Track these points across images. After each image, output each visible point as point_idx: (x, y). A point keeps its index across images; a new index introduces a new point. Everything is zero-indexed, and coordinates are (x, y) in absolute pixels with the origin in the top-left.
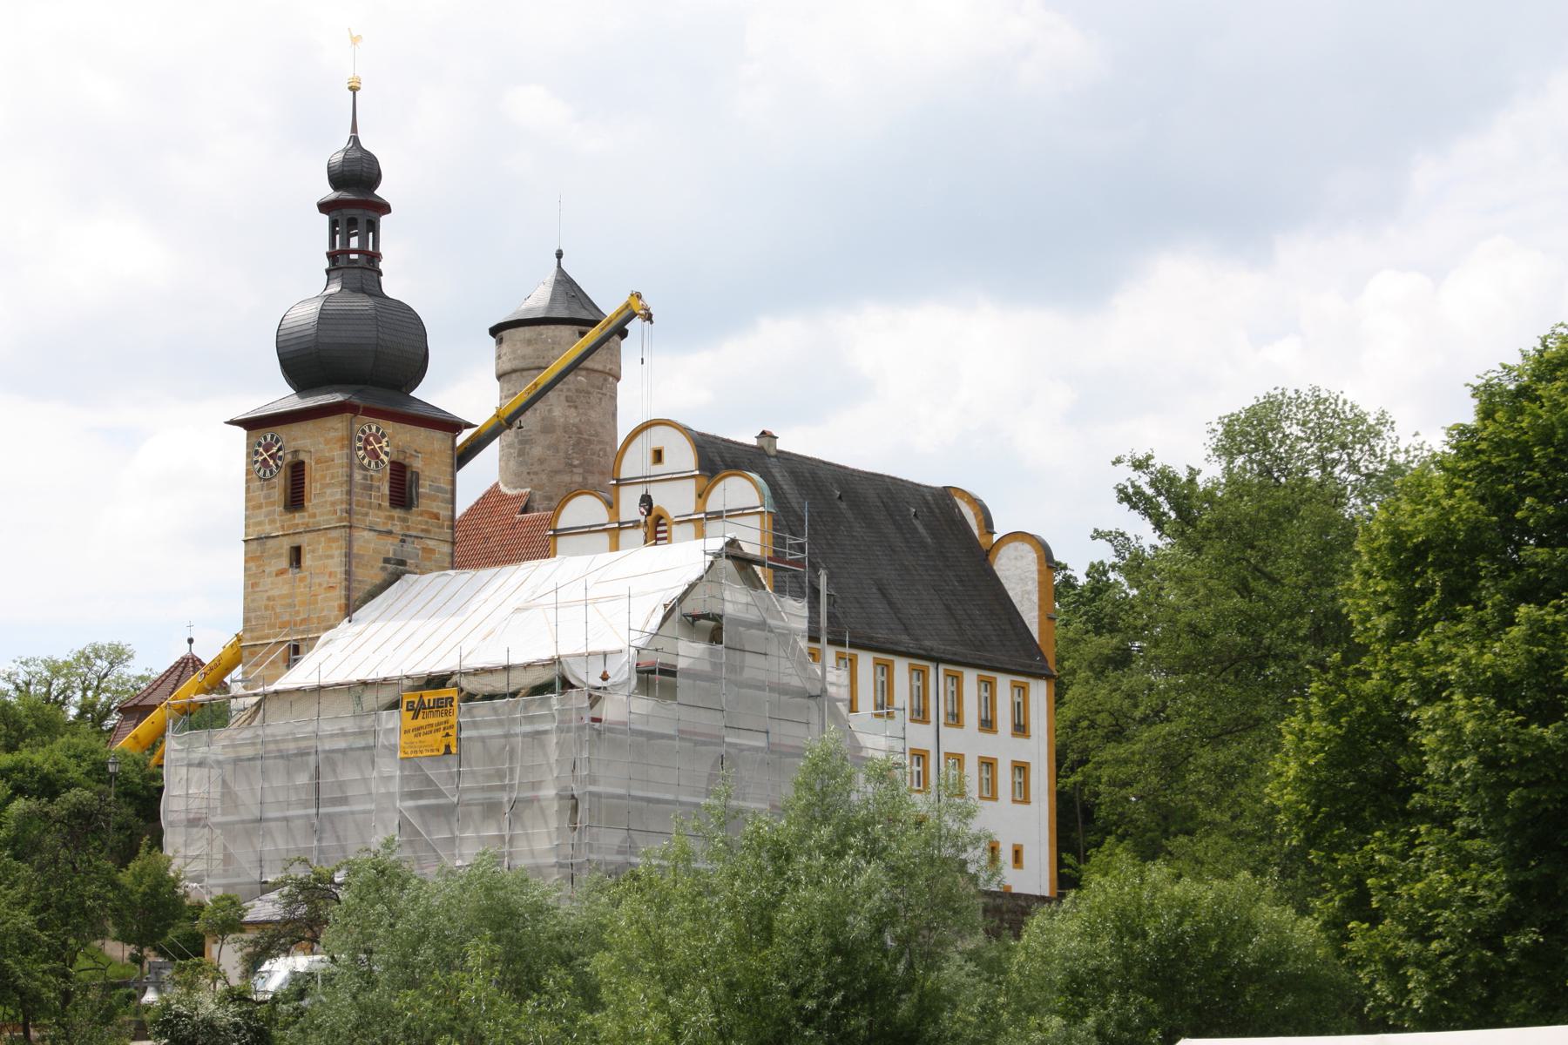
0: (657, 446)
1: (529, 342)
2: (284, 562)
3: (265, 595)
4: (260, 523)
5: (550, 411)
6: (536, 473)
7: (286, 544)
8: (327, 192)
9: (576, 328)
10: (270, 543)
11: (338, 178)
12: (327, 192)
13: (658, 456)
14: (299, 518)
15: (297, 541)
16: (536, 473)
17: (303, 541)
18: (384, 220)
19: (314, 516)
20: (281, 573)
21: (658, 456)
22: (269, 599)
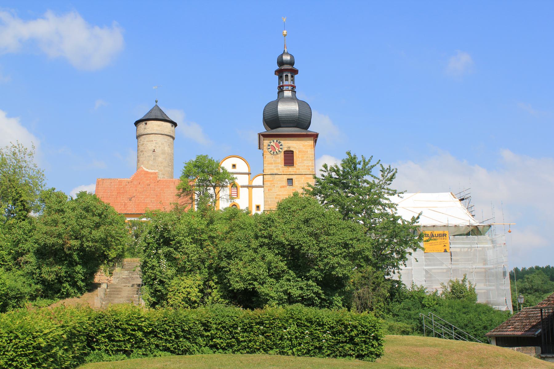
1: (159, 126)
2: (285, 183)
3: (276, 194)
7: (286, 177)
12: (277, 68)
14: (291, 170)
15: (290, 177)
19: (299, 169)
20: (284, 187)
21: (234, 166)
22: (277, 195)
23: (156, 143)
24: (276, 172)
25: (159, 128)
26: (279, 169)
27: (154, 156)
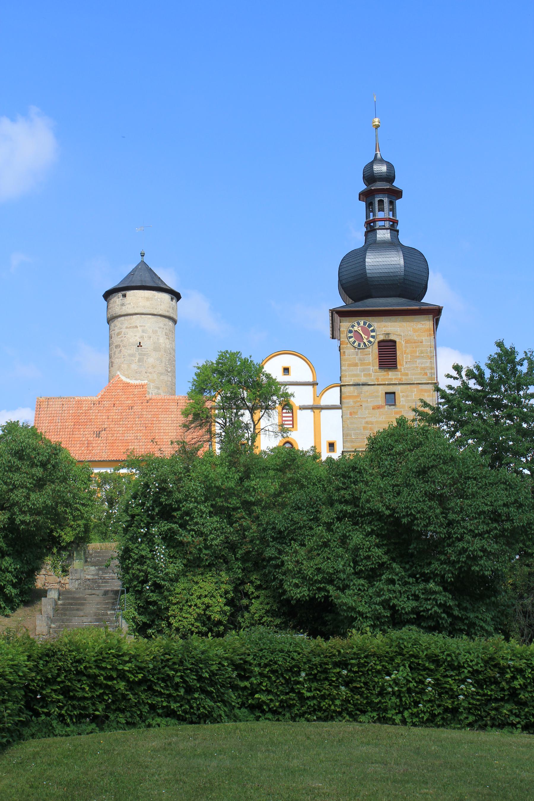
0: (286, 366)
2: (381, 401)
3: (364, 421)
4: (356, 375)
5: (158, 339)
6: (151, 373)
7: (382, 390)
8: (363, 187)
9: (120, 294)
10: (366, 388)
11: (370, 177)
12: (363, 187)
13: (286, 370)
14: (392, 376)
15: (391, 389)
16: (151, 373)
17: (397, 389)
18: (399, 203)
19: (407, 375)
20: (379, 407)
23: (143, 331)
24: (363, 380)
25: (148, 304)
26: (370, 375)
27: (140, 354)
